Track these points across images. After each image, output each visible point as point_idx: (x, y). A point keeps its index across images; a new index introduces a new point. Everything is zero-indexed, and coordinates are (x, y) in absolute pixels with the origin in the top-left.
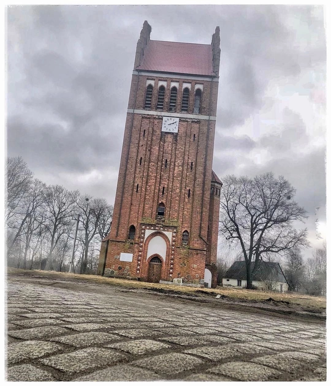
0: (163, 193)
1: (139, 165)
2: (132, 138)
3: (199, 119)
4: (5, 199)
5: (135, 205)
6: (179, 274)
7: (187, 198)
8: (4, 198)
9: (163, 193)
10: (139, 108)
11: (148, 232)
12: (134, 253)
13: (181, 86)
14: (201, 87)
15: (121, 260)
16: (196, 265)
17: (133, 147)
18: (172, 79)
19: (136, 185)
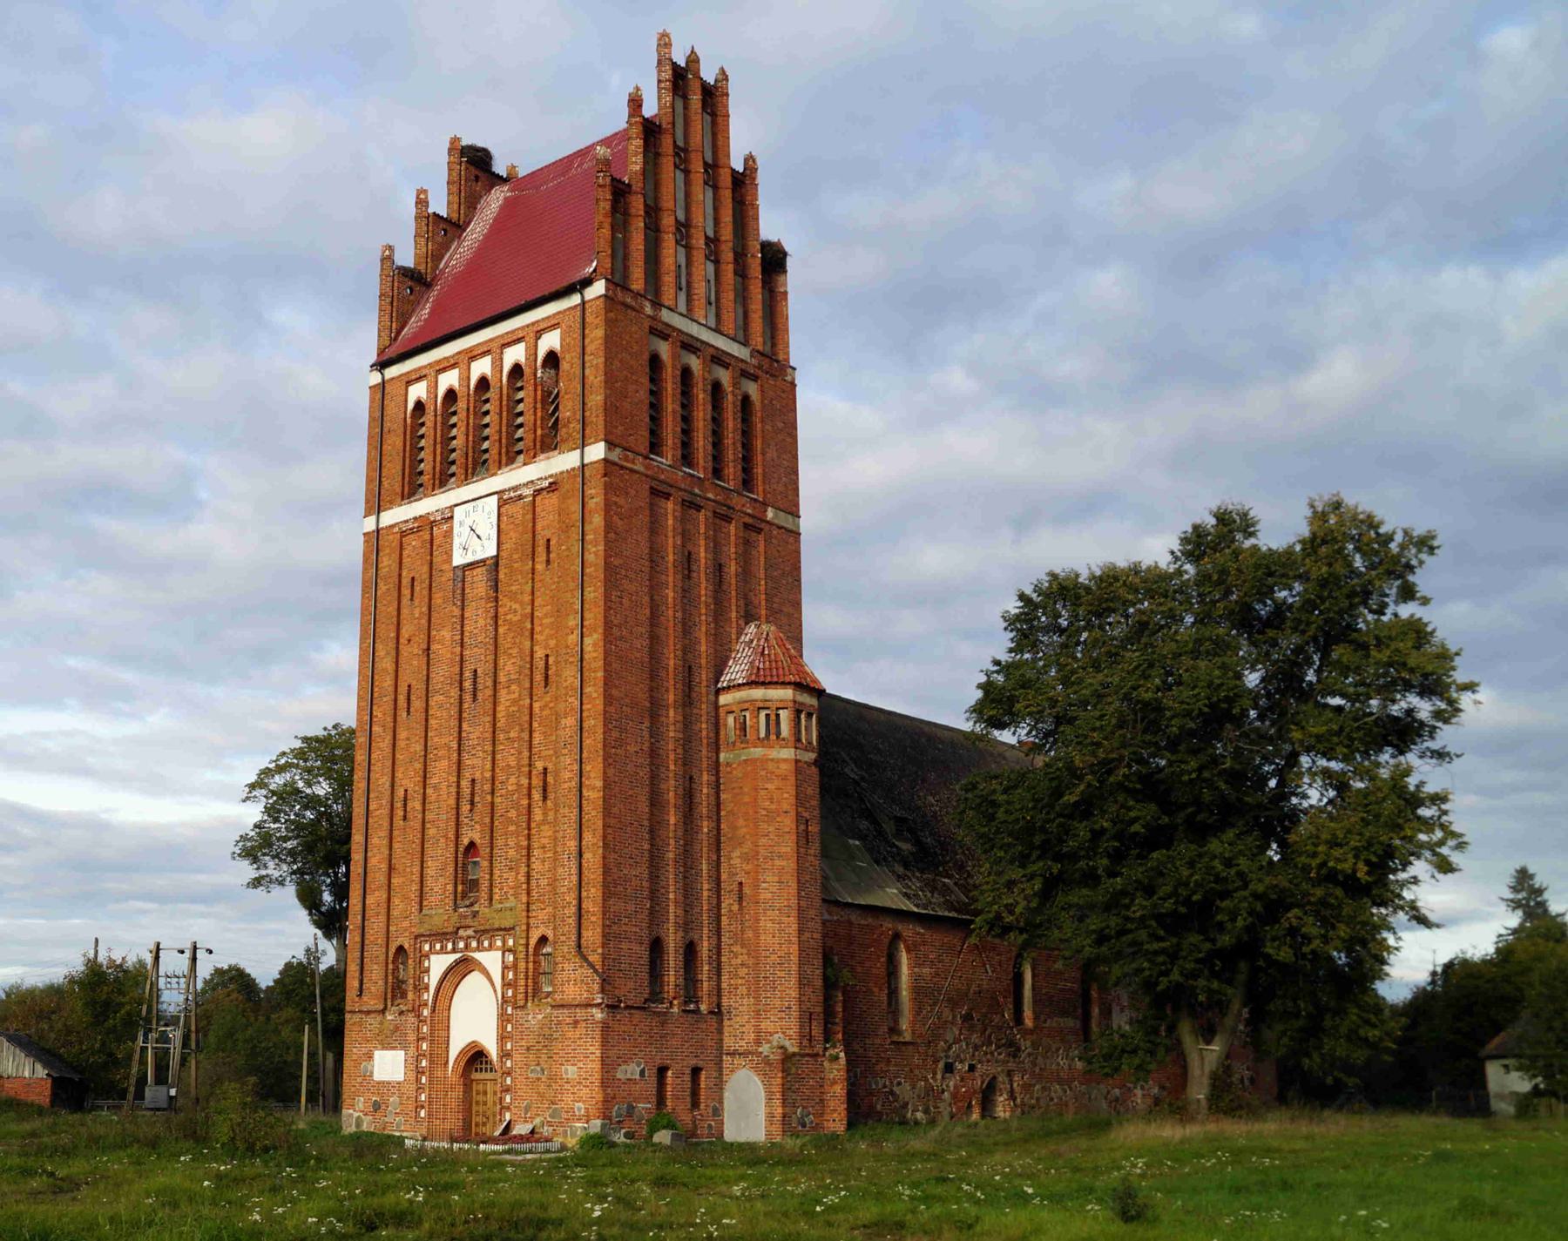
0: (472, 803)
1: (405, 714)
2: (533, 907)
3: (551, 476)
4: (785, 293)
5: (401, 870)
6: (527, 1109)
7: (540, 804)
8: (790, 297)
9: (472, 803)
10: (392, 504)
11: (439, 964)
12: (404, 1048)
13: (498, 364)
14: (551, 341)
15: (377, 1077)
16: (575, 1068)
17: (784, 766)
18: (471, 349)
19: (400, 793)
